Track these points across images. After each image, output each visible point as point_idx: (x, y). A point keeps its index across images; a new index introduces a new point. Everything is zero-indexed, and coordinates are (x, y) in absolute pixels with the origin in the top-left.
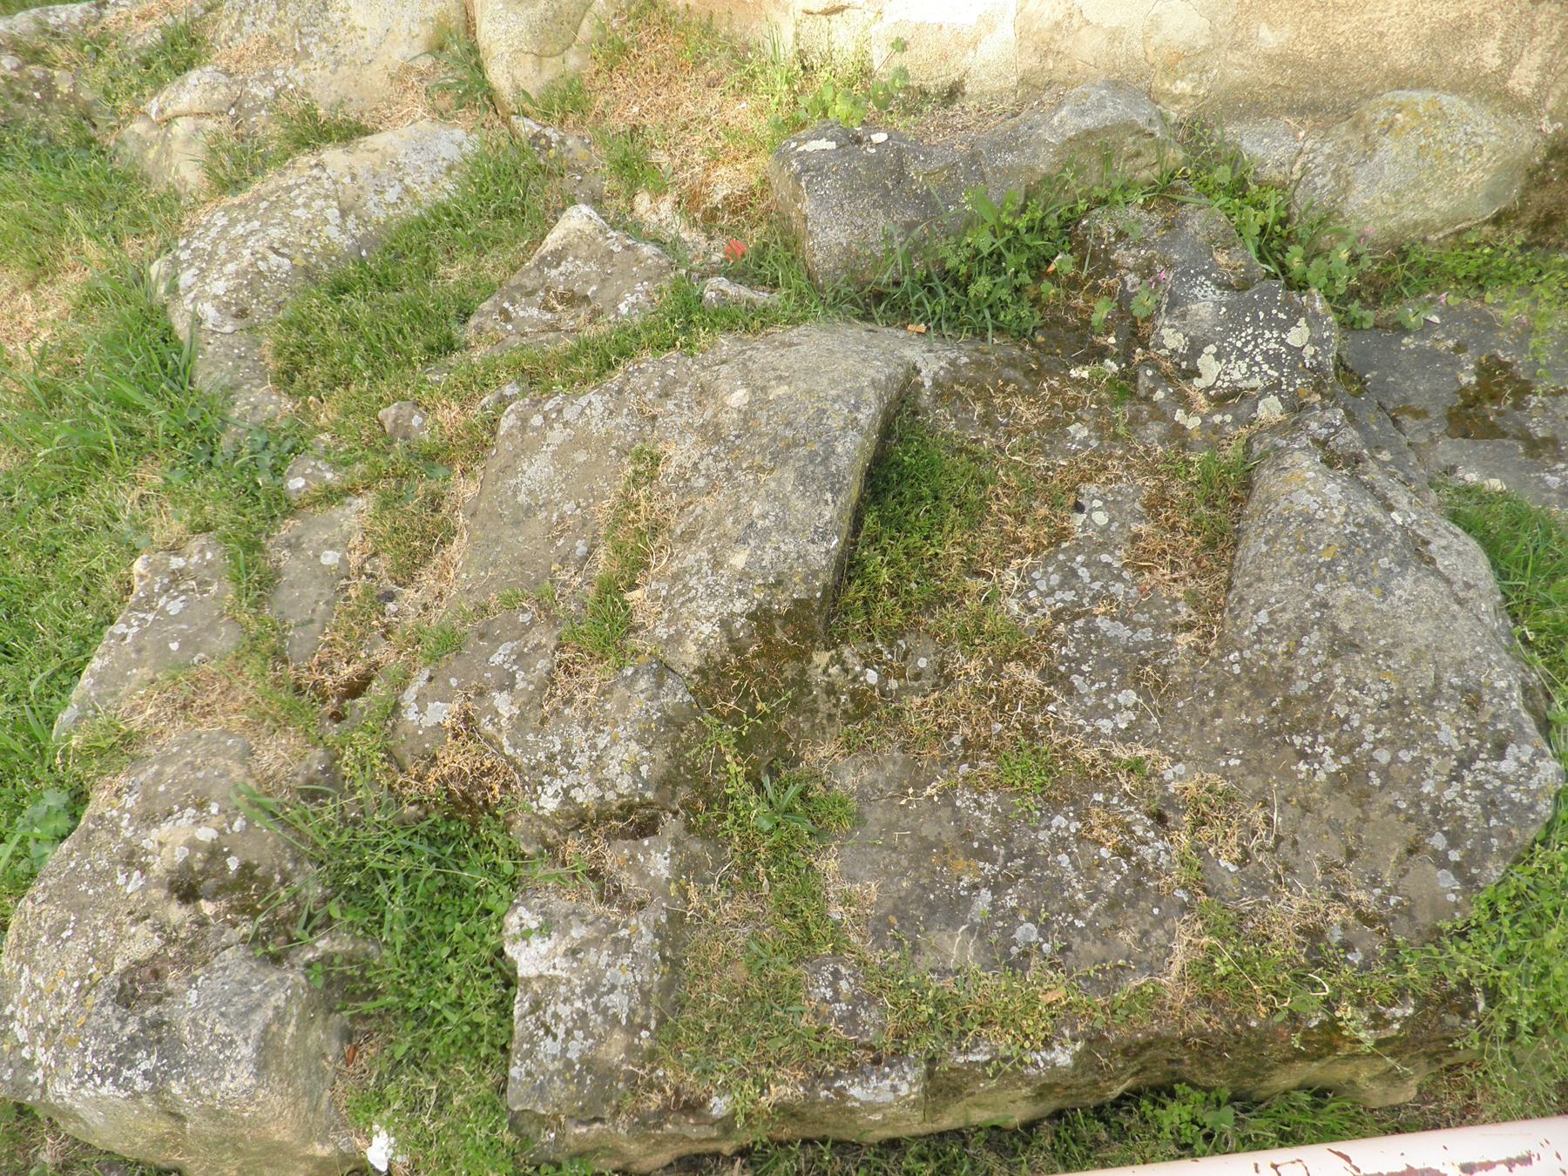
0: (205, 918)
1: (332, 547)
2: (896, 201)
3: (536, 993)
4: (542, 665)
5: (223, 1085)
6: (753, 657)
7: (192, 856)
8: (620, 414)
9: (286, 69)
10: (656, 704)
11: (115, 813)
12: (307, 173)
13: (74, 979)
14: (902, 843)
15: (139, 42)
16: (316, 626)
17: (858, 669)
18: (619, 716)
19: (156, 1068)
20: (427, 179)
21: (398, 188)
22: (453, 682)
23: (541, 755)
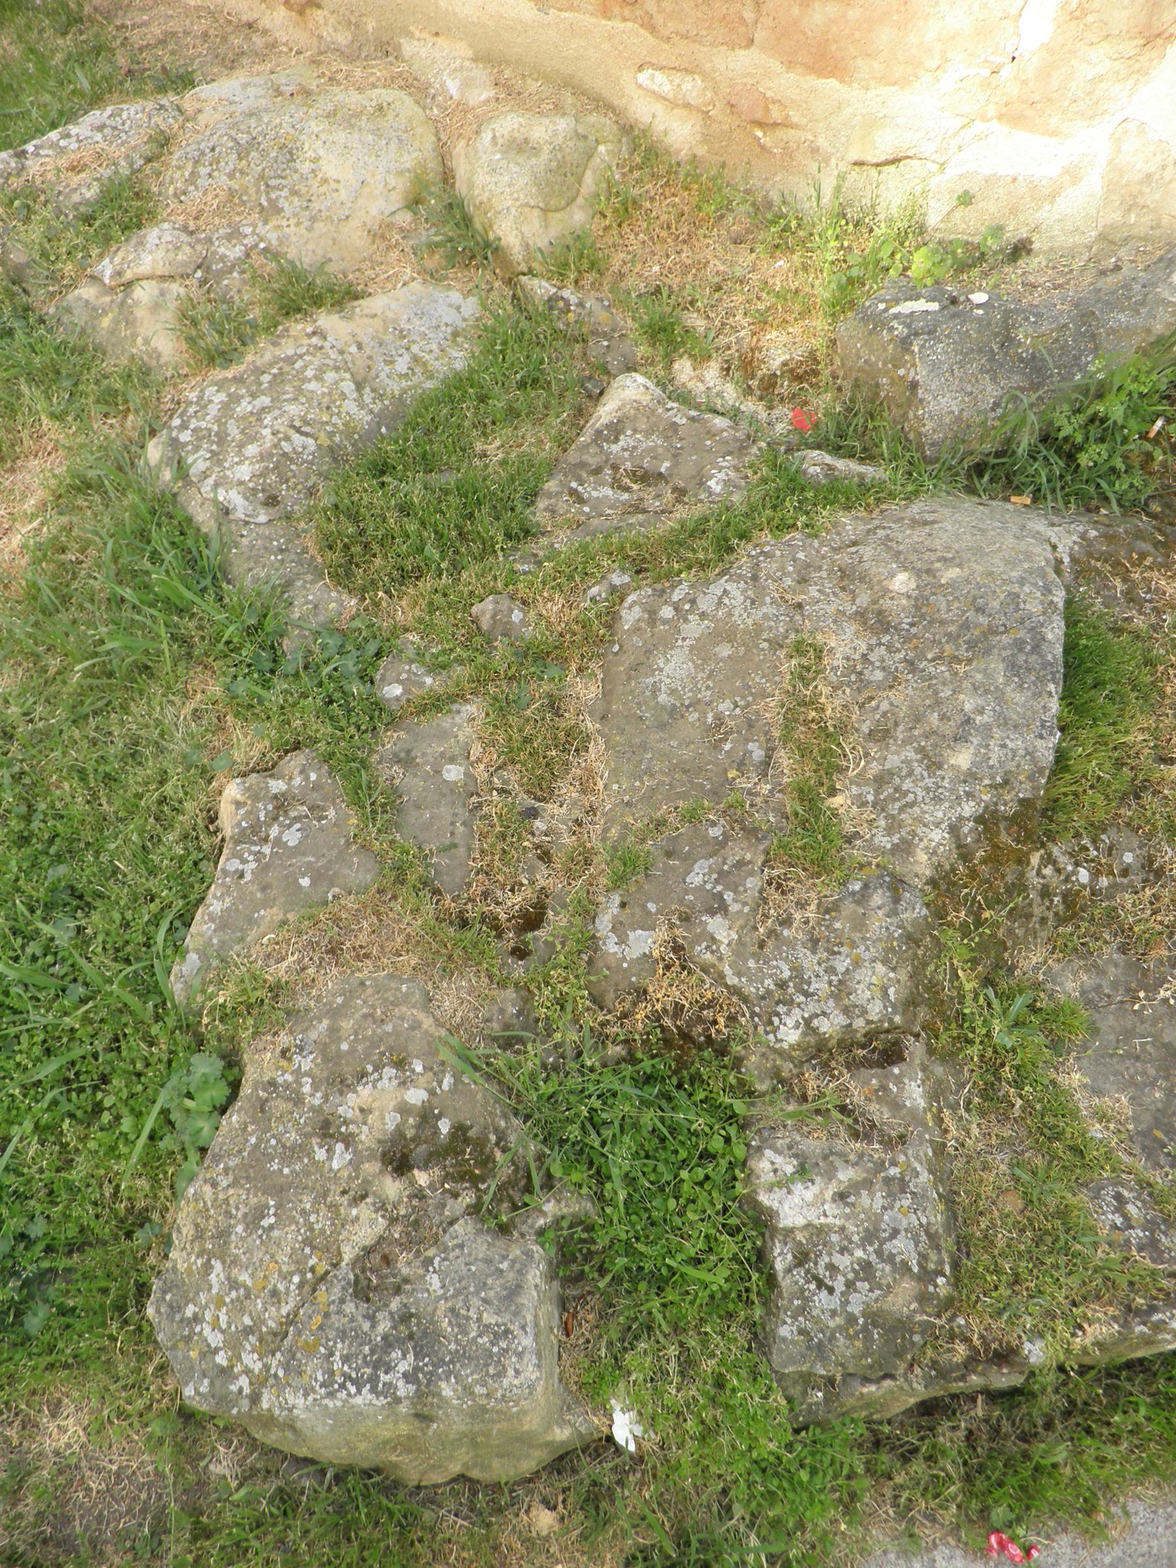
0: (421, 1189)
1: (452, 760)
2: (1001, 365)
3: (800, 1243)
4: (753, 883)
5: (506, 1382)
6: (981, 863)
7: (404, 1122)
8: (763, 603)
9: (255, 227)
10: (895, 920)
11: (289, 1078)
12: (305, 341)
13: (292, 1274)
14: (1144, 1050)
15: (76, 198)
16: (461, 851)
17: (1070, 868)
18: (857, 936)
19: (417, 1369)
20: (434, 347)
21: (407, 357)
22: (652, 907)
23: (769, 983)
